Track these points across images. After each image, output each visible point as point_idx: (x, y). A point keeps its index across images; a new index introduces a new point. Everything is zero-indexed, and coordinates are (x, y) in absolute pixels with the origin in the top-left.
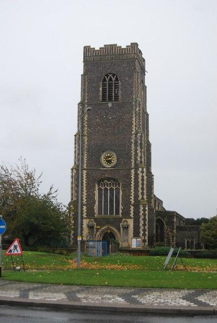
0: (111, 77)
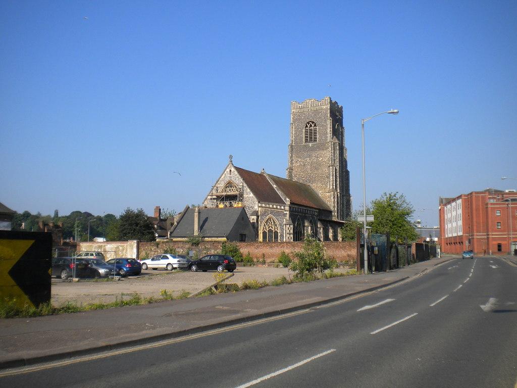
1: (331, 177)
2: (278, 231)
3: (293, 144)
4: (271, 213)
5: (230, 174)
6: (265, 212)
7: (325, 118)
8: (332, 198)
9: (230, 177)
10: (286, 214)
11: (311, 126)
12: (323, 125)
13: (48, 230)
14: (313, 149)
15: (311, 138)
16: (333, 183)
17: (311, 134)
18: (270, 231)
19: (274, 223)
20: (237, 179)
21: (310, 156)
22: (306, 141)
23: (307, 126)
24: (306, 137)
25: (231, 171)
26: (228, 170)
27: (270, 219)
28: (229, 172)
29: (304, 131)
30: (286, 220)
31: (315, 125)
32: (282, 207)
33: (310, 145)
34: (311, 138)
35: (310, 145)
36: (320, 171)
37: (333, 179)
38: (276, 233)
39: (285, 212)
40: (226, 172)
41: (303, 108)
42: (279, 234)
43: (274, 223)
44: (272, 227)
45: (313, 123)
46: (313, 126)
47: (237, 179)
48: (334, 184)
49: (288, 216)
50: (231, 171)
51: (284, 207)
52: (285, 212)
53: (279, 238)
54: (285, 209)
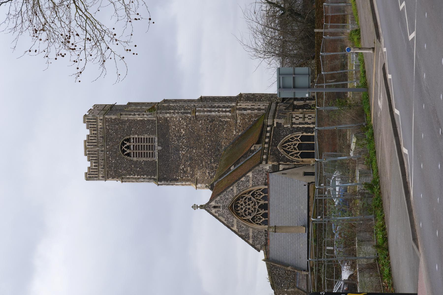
0: (126, 147)
2: (301, 135)
3: (156, 177)
4: (276, 146)
5: (220, 207)
6: (274, 154)
7: (118, 124)
8: (245, 112)
9: (224, 207)
10: (277, 123)
11: (128, 147)
12: (130, 127)
13: (324, 5)
16: (223, 111)
18: (300, 147)
19: (289, 141)
20: (227, 197)
21: (177, 150)
23: (128, 155)
25: (215, 207)
27: (283, 147)
28: (216, 209)
29: (135, 159)
30: (286, 123)
31: (128, 140)
32: (269, 129)
35: (160, 148)
36: (202, 133)
37: (215, 111)
39: (275, 125)
40: (217, 215)
41: (98, 160)
42: (305, 134)
43: (289, 141)
44: (295, 144)
45: (123, 144)
46: (128, 144)
47: (227, 197)
48: (224, 110)
49: (280, 121)
50: (215, 207)
51: (268, 126)
52: (275, 125)
54: (270, 126)
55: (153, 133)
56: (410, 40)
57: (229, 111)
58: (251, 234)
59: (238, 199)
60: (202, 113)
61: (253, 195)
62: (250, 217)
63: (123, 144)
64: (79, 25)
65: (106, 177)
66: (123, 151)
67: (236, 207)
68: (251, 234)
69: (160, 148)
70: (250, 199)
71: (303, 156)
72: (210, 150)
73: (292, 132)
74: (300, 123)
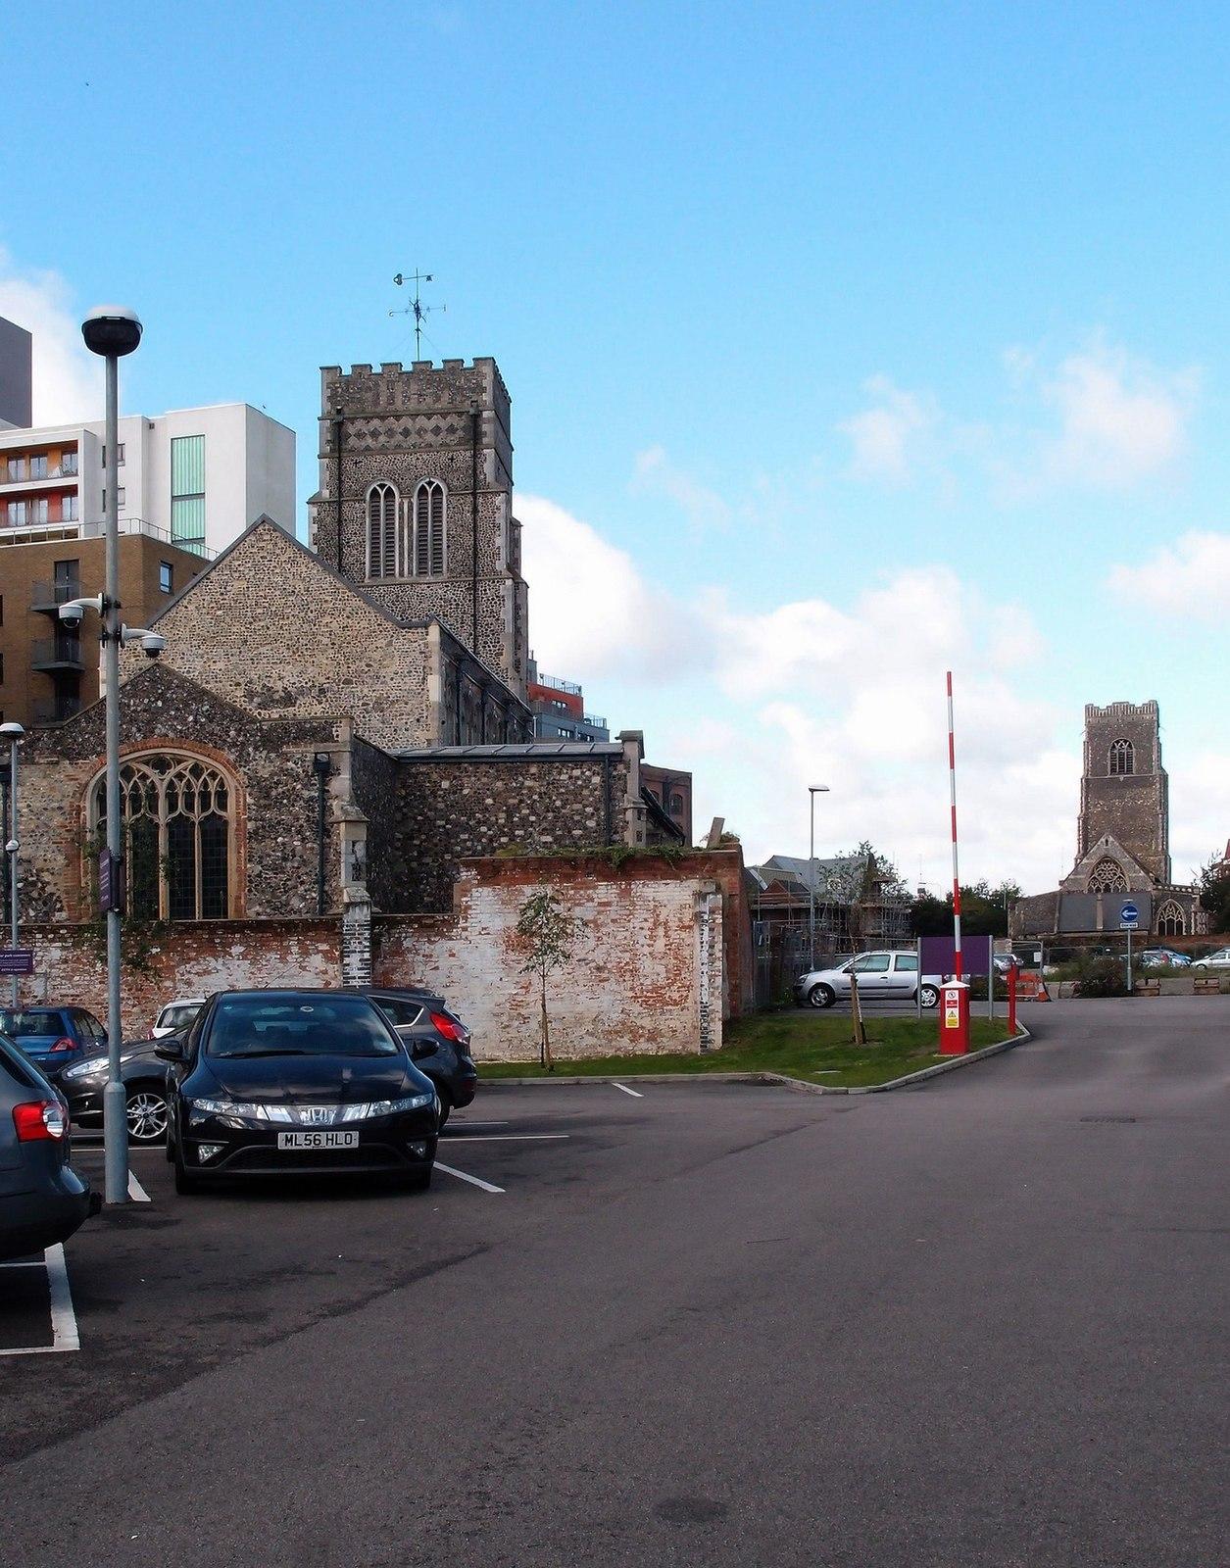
1: (1161, 832)
8: (1162, 864)
12: (1144, 747)
14: (1126, 784)
15: (1122, 767)
17: (1121, 759)
21: (1121, 797)
22: (1113, 771)
24: (1113, 765)
25: (1107, 841)
26: (1103, 840)
29: (1109, 754)
31: (1130, 746)
33: (1122, 778)
34: (1122, 767)
35: (1122, 779)
38: (1180, 924)
42: (1184, 925)
43: (1177, 910)
49: (1198, 901)
50: (1107, 841)
53: (1184, 929)
55: (1138, 772)
56: (149, 1200)
57: (1163, 849)
58: (1078, 877)
59: (1115, 863)
60: (1161, 821)
61: (1120, 877)
62: (1096, 875)
63: (1126, 741)
64: (474, 495)
65: (1089, 725)
66: (1118, 742)
67: (1107, 862)
68: (1078, 877)
69: (1122, 779)
70: (1115, 874)
71: (1162, 924)
72: (1120, 830)
73: (1186, 912)
74: (1196, 920)
